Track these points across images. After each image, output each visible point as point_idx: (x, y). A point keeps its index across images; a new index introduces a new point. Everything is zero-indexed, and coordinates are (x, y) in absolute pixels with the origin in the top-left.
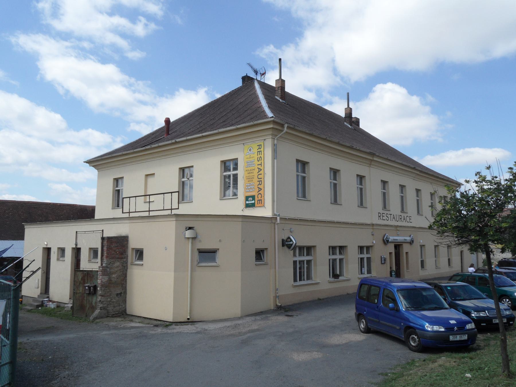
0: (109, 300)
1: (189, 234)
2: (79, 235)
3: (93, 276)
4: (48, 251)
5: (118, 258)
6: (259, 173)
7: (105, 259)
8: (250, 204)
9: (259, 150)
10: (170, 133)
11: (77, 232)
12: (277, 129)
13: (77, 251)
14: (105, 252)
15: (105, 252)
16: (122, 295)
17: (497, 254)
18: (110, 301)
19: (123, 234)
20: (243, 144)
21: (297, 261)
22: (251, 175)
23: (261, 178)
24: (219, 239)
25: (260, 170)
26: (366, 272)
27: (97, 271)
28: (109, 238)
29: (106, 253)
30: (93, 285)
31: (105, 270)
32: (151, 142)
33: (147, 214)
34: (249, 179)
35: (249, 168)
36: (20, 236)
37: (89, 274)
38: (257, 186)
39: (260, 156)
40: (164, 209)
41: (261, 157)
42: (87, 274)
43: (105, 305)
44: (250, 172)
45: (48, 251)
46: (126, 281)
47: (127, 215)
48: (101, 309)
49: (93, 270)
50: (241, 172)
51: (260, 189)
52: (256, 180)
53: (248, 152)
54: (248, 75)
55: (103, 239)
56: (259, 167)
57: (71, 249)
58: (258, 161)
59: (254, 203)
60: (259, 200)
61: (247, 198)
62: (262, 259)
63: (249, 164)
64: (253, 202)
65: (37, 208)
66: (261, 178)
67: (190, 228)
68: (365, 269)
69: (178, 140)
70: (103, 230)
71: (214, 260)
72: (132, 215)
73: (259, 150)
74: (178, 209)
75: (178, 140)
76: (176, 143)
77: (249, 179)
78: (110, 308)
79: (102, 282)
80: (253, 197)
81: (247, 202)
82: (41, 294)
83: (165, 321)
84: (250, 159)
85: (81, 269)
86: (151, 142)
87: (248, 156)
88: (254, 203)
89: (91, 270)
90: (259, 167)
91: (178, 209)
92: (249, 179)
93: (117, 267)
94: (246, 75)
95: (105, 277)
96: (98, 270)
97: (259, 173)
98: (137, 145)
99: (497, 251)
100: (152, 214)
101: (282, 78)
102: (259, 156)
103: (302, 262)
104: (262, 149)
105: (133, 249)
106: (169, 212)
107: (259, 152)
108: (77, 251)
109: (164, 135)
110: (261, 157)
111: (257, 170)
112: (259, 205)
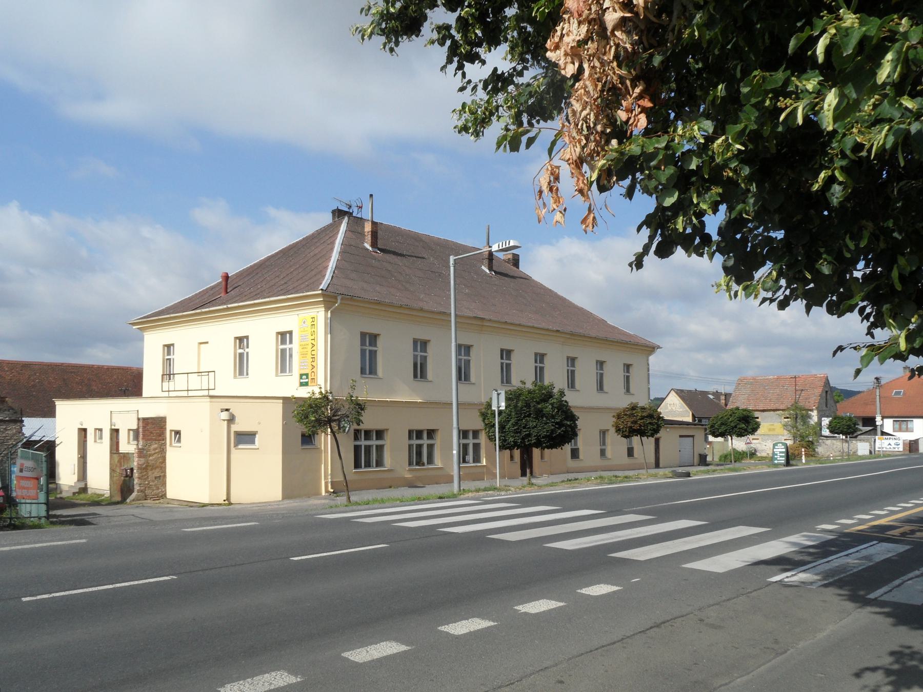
0: (147, 482)
1: (225, 415)
2: (113, 415)
3: (130, 458)
4: (83, 432)
5: (155, 440)
6: (313, 349)
7: (141, 440)
8: (304, 383)
9: (313, 323)
10: (228, 291)
11: (111, 412)
12: (330, 301)
13: (115, 432)
14: (141, 434)
15: (141, 434)
16: (162, 478)
17: (762, 443)
18: (148, 484)
19: (162, 415)
20: (298, 315)
21: (361, 445)
22: (305, 350)
23: (314, 355)
24: (257, 421)
25: (313, 345)
26: (471, 460)
27: (133, 453)
28: (145, 419)
29: (142, 435)
30: (129, 467)
31: (141, 453)
32: (207, 301)
33: (185, 394)
34: (303, 354)
35: (303, 343)
36: (50, 412)
37: (126, 457)
38: (310, 363)
39: (314, 330)
40: (170, 396)
41: (314, 331)
42: (124, 456)
43: (142, 488)
44: (303, 347)
45: (83, 432)
46: (165, 465)
47: (166, 394)
48: (138, 492)
49: (130, 452)
50: (296, 346)
51: (313, 367)
52: (309, 356)
53: (302, 325)
54: (339, 208)
55: (139, 419)
56: (313, 342)
57: (77, 429)
58: (312, 335)
59: (308, 382)
60: (313, 379)
61: (301, 375)
62: (312, 443)
63: (303, 338)
64: (307, 380)
65: (74, 372)
66: (314, 355)
67: (227, 410)
68: (470, 457)
69: (229, 306)
70: (138, 411)
71: (253, 442)
72: (172, 394)
73: (313, 323)
74: (215, 389)
75: (229, 306)
76: (228, 309)
77: (303, 354)
78: (148, 492)
79: (138, 464)
80: (307, 375)
81: (302, 381)
82: (78, 481)
83: (197, 503)
84: (305, 333)
85: (120, 452)
86: (207, 301)
87: (302, 329)
88: (308, 382)
89: (127, 452)
90: (313, 342)
91: (215, 389)
92: (303, 355)
93: (155, 449)
94: (336, 208)
95: (142, 459)
96: (133, 452)
97: (313, 349)
98: (190, 304)
99: (762, 439)
100: (191, 394)
101: (374, 220)
102: (313, 330)
103: (368, 449)
104: (315, 323)
105: (171, 431)
106: (206, 393)
107: (312, 325)
108: (115, 432)
109: (221, 293)
110: (314, 331)
111: (311, 345)
112: (313, 384)
